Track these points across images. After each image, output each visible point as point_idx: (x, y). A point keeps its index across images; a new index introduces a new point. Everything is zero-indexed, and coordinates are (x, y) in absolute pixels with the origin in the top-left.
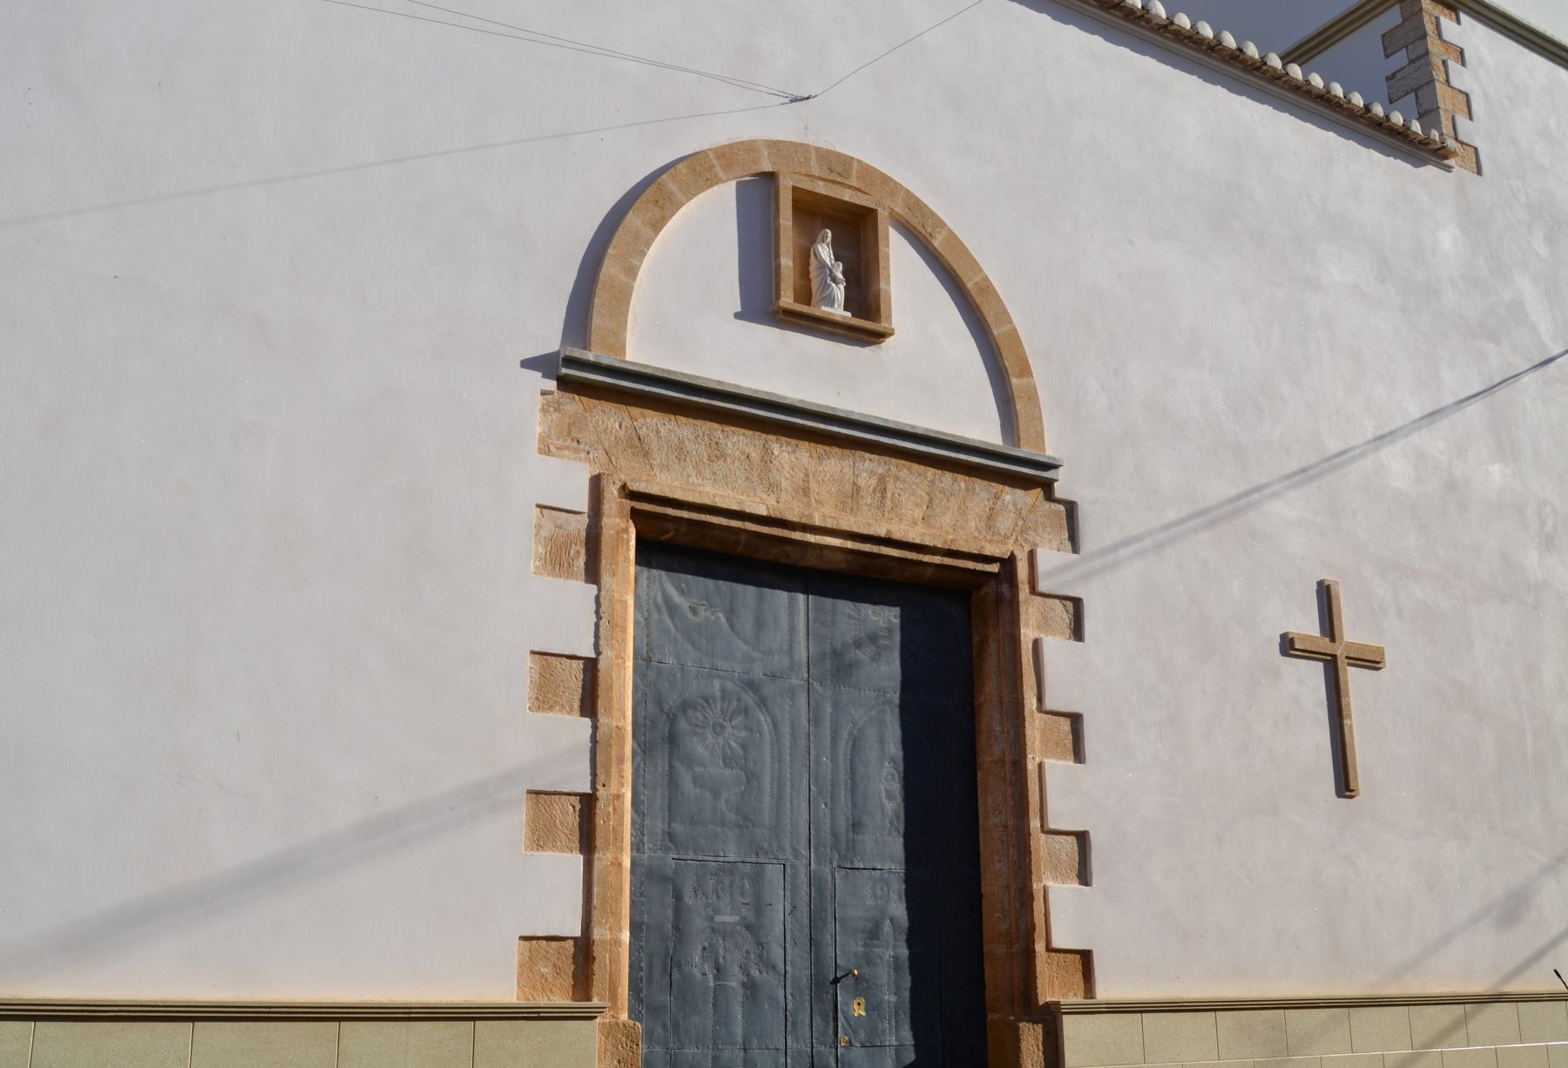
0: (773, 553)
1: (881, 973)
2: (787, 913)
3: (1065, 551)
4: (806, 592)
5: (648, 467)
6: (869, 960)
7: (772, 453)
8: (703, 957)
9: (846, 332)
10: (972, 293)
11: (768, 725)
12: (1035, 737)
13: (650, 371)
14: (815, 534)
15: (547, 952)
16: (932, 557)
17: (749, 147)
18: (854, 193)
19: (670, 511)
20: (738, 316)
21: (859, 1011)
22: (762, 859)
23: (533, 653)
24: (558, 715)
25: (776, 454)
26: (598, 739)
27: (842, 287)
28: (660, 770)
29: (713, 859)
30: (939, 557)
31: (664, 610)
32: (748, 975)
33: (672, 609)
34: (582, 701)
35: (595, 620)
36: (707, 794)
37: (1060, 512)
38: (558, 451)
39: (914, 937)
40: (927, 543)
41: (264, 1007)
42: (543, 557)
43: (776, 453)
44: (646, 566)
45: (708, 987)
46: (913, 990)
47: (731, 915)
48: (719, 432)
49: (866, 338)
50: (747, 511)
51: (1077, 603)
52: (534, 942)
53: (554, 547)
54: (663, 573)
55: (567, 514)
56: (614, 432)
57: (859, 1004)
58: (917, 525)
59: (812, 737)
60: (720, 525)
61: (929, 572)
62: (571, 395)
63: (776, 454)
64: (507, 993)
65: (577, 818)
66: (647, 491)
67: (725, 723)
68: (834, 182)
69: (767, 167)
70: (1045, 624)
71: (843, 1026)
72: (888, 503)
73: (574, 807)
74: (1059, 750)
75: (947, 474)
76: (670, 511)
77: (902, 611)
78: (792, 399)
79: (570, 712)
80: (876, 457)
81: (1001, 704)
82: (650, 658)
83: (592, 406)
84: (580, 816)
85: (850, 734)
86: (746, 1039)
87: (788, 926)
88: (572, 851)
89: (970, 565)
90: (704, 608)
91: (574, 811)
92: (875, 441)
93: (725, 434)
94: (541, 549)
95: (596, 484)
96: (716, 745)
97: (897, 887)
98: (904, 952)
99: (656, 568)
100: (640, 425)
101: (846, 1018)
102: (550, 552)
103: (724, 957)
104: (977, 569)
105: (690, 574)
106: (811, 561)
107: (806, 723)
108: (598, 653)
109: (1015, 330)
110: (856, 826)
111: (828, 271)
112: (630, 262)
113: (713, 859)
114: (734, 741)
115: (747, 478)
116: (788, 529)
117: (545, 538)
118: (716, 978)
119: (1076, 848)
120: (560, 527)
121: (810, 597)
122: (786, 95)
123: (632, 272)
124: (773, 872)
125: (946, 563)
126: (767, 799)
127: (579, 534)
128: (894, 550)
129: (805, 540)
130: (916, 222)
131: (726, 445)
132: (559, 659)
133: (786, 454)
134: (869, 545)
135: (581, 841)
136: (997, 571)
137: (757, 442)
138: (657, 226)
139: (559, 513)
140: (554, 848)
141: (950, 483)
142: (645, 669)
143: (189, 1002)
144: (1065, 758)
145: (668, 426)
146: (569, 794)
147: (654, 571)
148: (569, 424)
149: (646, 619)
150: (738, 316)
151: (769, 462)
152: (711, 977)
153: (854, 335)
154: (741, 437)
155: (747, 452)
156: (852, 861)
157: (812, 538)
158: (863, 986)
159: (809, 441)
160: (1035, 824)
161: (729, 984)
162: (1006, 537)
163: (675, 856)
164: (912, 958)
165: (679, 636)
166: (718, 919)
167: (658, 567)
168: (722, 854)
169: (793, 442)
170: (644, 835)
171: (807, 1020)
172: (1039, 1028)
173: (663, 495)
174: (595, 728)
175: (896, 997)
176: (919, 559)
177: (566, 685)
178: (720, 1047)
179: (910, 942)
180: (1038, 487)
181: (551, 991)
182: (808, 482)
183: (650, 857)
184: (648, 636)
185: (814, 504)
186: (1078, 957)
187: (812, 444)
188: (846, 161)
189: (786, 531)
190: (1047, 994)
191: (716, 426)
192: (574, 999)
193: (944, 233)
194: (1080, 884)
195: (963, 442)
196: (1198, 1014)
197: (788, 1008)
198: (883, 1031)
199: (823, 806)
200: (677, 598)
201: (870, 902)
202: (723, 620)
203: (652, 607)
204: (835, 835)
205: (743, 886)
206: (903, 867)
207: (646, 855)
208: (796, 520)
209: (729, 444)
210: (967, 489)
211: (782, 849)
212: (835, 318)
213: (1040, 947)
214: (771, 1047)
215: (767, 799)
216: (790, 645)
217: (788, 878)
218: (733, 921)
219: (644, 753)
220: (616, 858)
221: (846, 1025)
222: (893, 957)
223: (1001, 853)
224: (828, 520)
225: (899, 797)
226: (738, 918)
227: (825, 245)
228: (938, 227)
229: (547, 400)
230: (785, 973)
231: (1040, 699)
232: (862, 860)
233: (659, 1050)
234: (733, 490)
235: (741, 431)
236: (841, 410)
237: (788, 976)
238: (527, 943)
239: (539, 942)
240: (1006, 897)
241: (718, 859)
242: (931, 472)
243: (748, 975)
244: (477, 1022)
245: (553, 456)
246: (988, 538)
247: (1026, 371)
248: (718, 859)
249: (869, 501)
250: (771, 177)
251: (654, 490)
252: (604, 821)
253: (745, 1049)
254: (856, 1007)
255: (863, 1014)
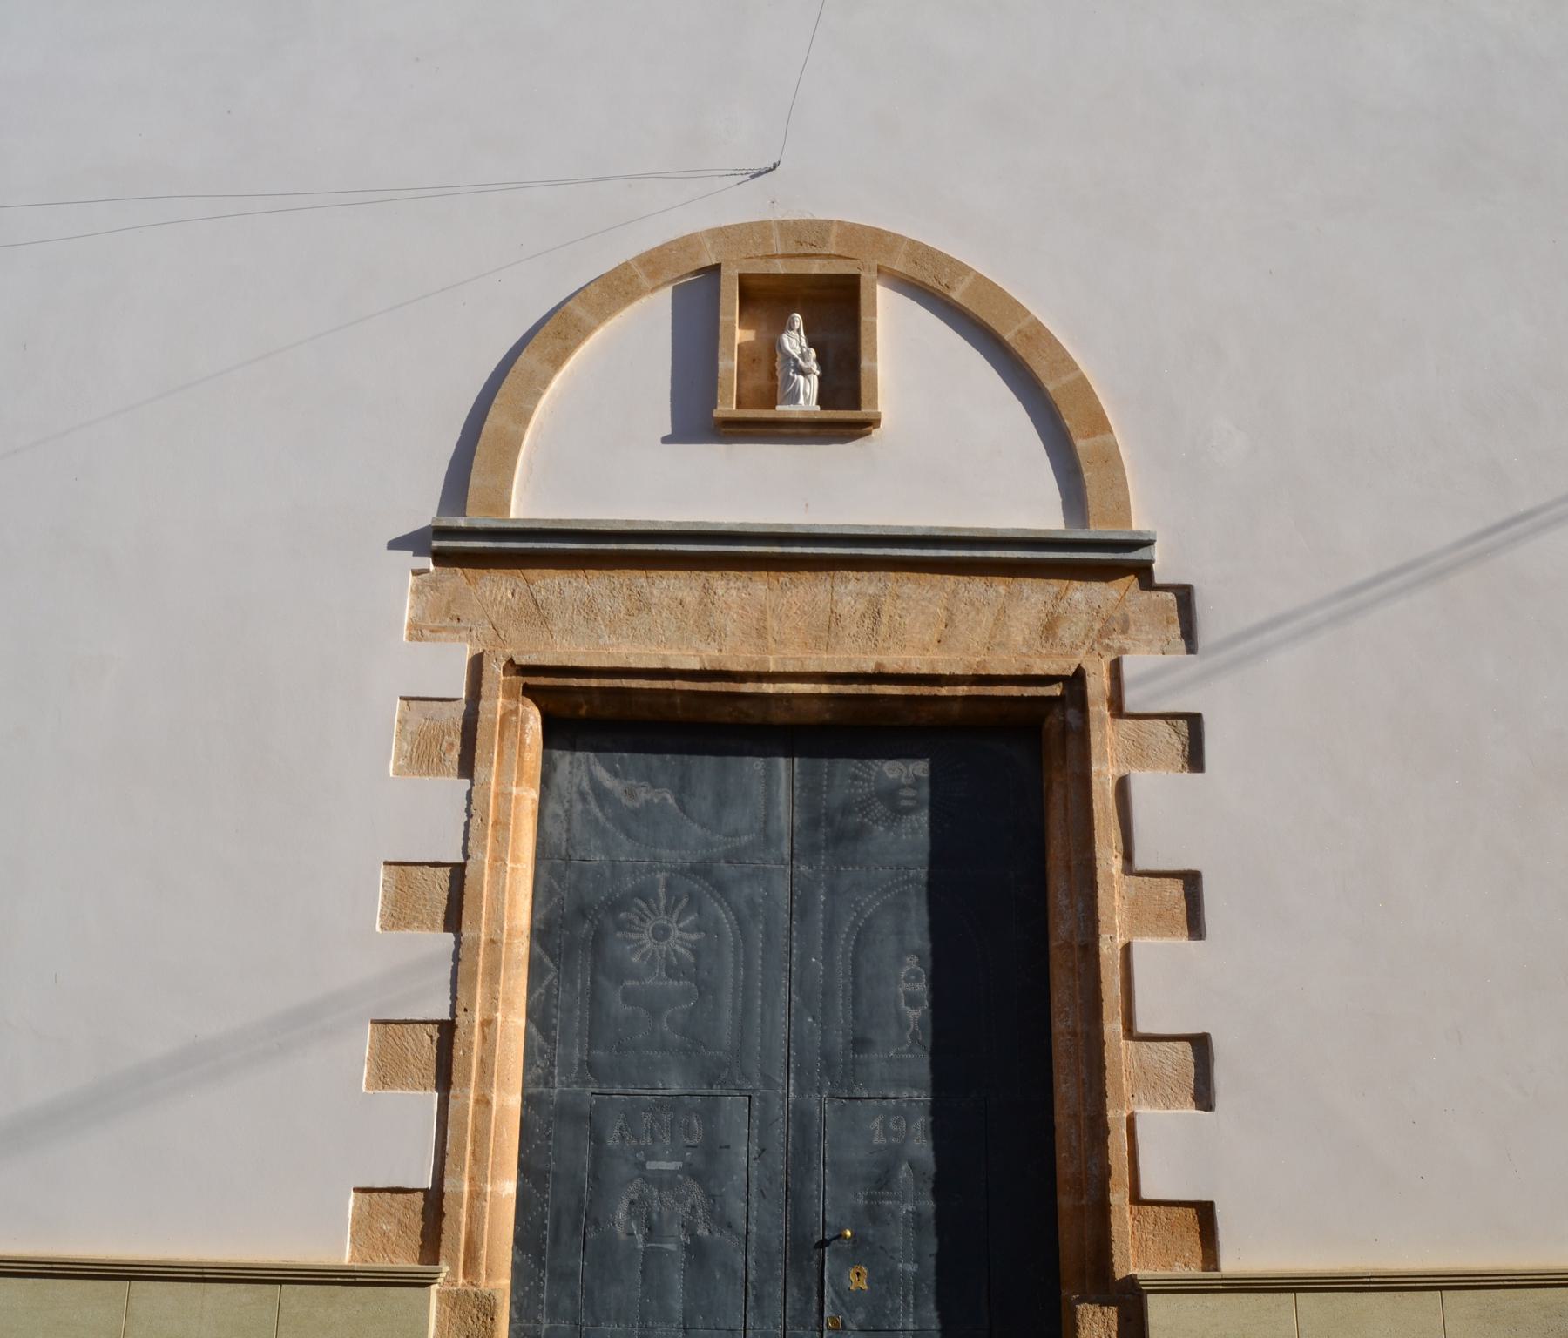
0: (725, 714)
1: (893, 1233)
2: (752, 1157)
3: (1176, 652)
4: (789, 754)
5: (546, 634)
6: (873, 1214)
7: (715, 593)
8: (629, 1213)
9: (815, 430)
10: (1013, 345)
11: (731, 924)
12: (1114, 909)
13: (536, 526)
14: (774, 683)
15: (391, 1206)
16: (953, 688)
17: (687, 244)
18: (825, 262)
19: (574, 682)
20: (666, 440)
21: (857, 1280)
22: (716, 1090)
23: (386, 863)
24: (417, 932)
25: (720, 594)
26: (460, 957)
27: (814, 379)
28: (579, 986)
29: (649, 1092)
30: (965, 688)
31: (591, 798)
32: (693, 1235)
33: (601, 794)
34: (448, 913)
35: (466, 819)
36: (643, 1013)
37: (1167, 602)
38: (433, 635)
39: (942, 1186)
40: (941, 672)
41: (170, 1267)
42: (408, 755)
43: (720, 592)
44: (567, 750)
45: (635, 1249)
46: (940, 1257)
47: (670, 1161)
48: (642, 580)
49: (846, 431)
50: (672, 667)
51: (1194, 722)
52: (375, 1195)
53: (422, 741)
54: (592, 755)
55: (440, 703)
56: (504, 601)
57: (858, 1274)
58: (928, 650)
59: (795, 934)
60: (642, 689)
61: (956, 708)
62: (452, 570)
63: (720, 594)
64: (345, 1256)
65: (435, 1049)
66: (538, 663)
67: (670, 925)
68: (806, 256)
69: (709, 260)
70: (1141, 754)
71: (832, 1302)
72: (883, 629)
73: (431, 1037)
74: (1161, 924)
75: (977, 579)
76: (574, 682)
77: (932, 768)
78: (728, 524)
79: (432, 928)
80: (866, 575)
81: (1069, 868)
82: (570, 856)
83: (478, 577)
84: (437, 1048)
85: (854, 925)
86: (688, 1316)
87: (754, 1173)
88: (425, 1089)
89: (1014, 691)
90: (644, 789)
91: (432, 1041)
92: (969, 557)
93: (650, 580)
94: (405, 746)
95: (477, 666)
96: (657, 953)
97: (921, 1122)
98: (928, 1205)
99: (581, 751)
100: (537, 589)
101: (837, 1293)
102: (418, 748)
103: (659, 1213)
104: (1026, 695)
105: (627, 751)
106: (779, 716)
107: (786, 916)
108: (466, 856)
109: (1083, 379)
110: (860, 1043)
111: (792, 362)
112: (521, 408)
113: (649, 1092)
114: (681, 946)
115: (679, 628)
116: (735, 682)
117: (412, 733)
118: (647, 1239)
119: (1191, 1058)
120: (431, 719)
121: (796, 760)
122: (744, 172)
123: (524, 418)
124: (734, 1108)
125: (976, 693)
126: (727, 1015)
127: (454, 724)
128: (893, 687)
129: (760, 691)
130: (925, 276)
131: (651, 593)
132: (421, 868)
133: (734, 592)
134: (855, 686)
135: (437, 1077)
136: (1059, 694)
137: (694, 584)
138: (557, 362)
139: (429, 702)
140: (404, 1085)
141: (982, 590)
142: (563, 869)
143: (23, 1257)
144: (1173, 934)
145: (575, 584)
146: (425, 1022)
147: (579, 754)
148: (449, 603)
149: (566, 811)
150: (666, 440)
151: (710, 605)
152: (639, 1238)
153: (824, 431)
154: (673, 581)
155: (680, 597)
156: (850, 1089)
157: (769, 688)
158: (861, 1249)
159: (767, 570)
160: (1113, 1027)
161: (665, 1246)
162: (1073, 647)
163: (597, 1091)
164: (939, 1214)
165: (609, 826)
166: (651, 1165)
167: (583, 749)
168: (660, 1085)
169: (745, 575)
170: (554, 1066)
171: (779, 1293)
172: (1112, 1313)
173: (560, 664)
174: (458, 943)
175: (916, 1266)
176: (933, 693)
177: (427, 897)
178: (650, 1324)
179: (938, 1192)
180: (1129, 574)
181: (394, 1252)
182: (765, 620)
183: (562, 1093)
184: (568, 830)
185: (772, 645)
186: (1192, 1211)
187: (772, 573)
188: (823, 227)
189: (732, 684)
190: (1129, 1261)
191: (637, 573)
192: (421, 1262)
193: (968, 280)
194: (1197, 1108)
195: (987, 535)
196: (1261, 1295)
197: (750, 1278)
198: (895, 1311)
199: (810, 1020)
200: (608, 781)
201: (879, 1140)
202: (671, 801)
203: (575, 796)
204: (826, 1056)
205: (689, 1125)
206: (929, 1094)
207: (556, 1091)
208: (742, 669)
209: (655, 592)
210: (1010, 594)
211: (748, 1078)
212: (792, 416)
213: (1118, 1197)
214: (722, 1326)
215: (727, 1015)
216: (765, 822)
217: (755, 1113)
218: (673, 1168)
219: (558, 968)
220: (484, 1096)
221: (837, 1301)
222: (913, 1213)
223: (1067, 1070)
224: (788, 662)
225: (927, 1002)
226: (680, 1164)
227: (794, 333)
228: (959, 275)
229: (422, 579)
230: (747, 1233)
231: (1128, 856)
232: (866, 1087)
233: (565, 1325)
234: (658, 645)
235: (672, 573)
236: (799, 525)
237: (752, 1237)
238: (367, 1196)
239: (382, 1195)
240: (1073, 1131)
241: (655, 1092)
242: (950, 581)
243: (693, 1235)
244: (1298, 1294)
245: (427, 640)
246: (1044, 652)
247: (1100, 424)
248: (655, 1092)
249: (854, 630)
250: (715, 269)
251: (549, 660)
252: (464, 1052)
253: (685, 1328)
254: (853, 1278)
255: (866, 1287)
